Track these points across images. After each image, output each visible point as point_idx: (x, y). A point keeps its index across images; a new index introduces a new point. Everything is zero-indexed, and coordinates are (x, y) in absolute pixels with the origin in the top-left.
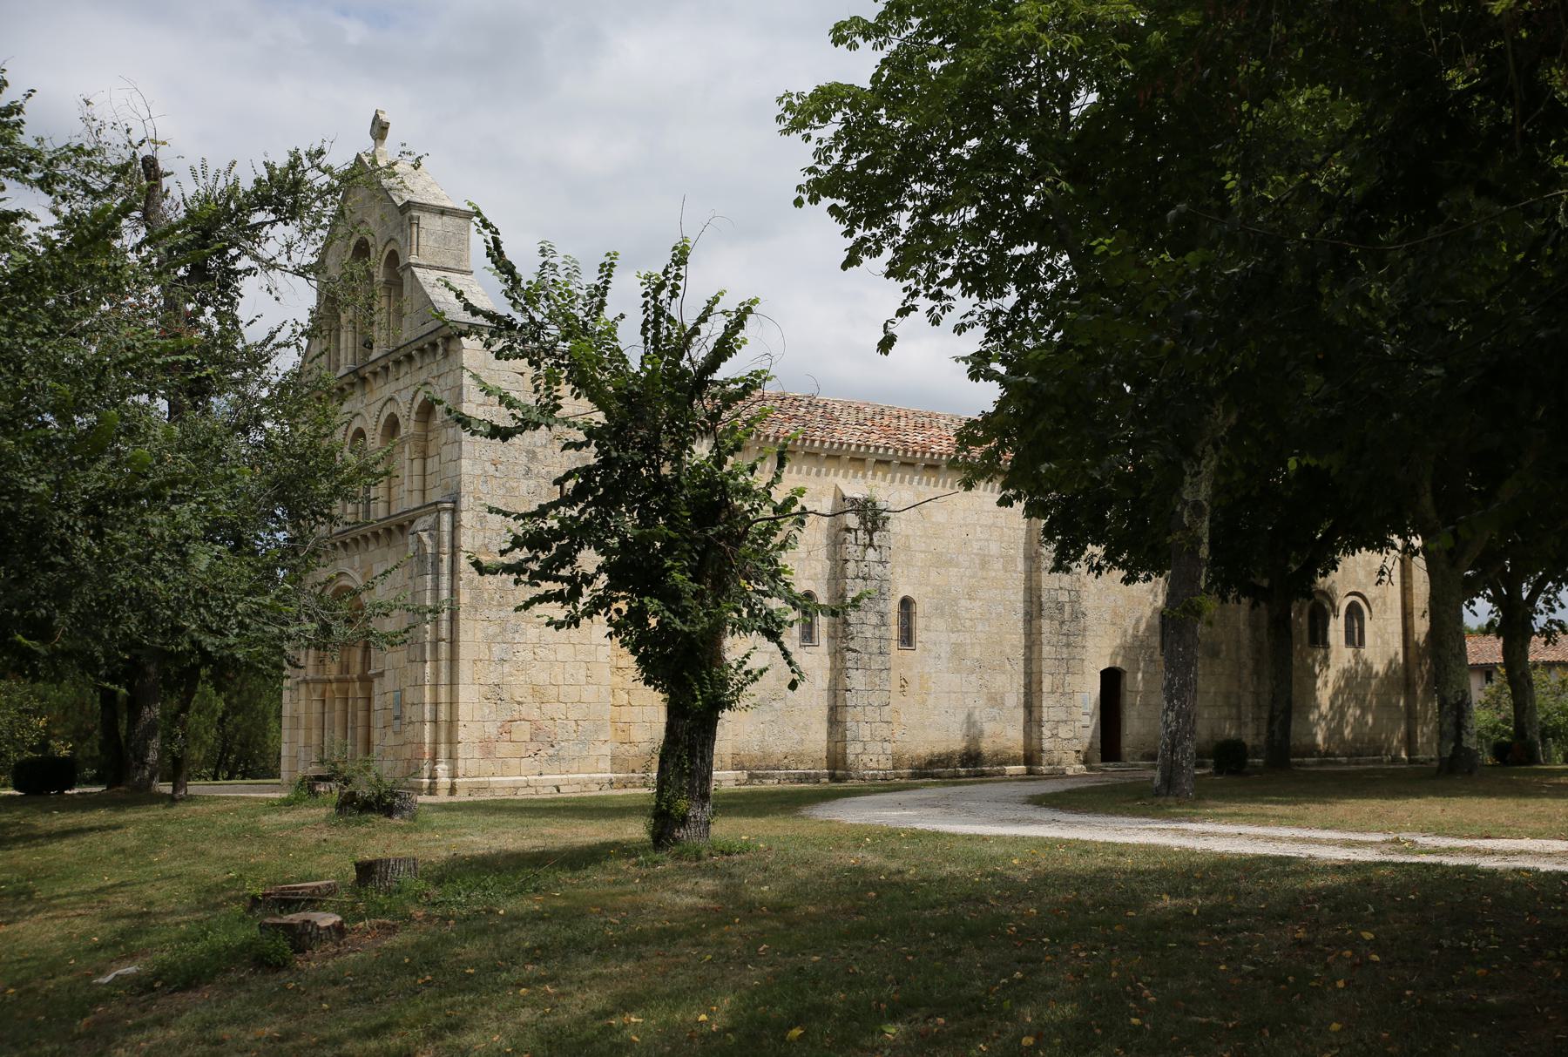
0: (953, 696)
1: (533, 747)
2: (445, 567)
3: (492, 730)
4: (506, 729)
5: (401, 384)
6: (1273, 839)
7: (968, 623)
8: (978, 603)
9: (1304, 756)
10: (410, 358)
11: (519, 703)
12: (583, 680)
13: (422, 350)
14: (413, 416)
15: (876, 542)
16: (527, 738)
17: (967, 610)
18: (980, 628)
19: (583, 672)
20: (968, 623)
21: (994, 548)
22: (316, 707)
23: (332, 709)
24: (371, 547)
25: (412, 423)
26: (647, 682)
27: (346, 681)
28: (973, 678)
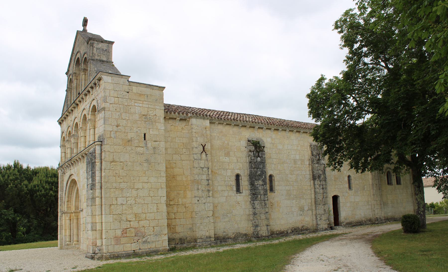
0: (288, 208)
1: (136, 238)
2: (98, 164)
3: (119, 233)
4: (125, 231)
5: (87, 102)
6: (67, 183)
7: (291, 183)
8: (294, 176)
9: (68, 197)
10: (89, 92)
11: (130, 221)
12: (156, 211)
13: (92, 88)
14: (90, 113)
15: (260, 155)
16: (134, 235)
17: (291, 178)
18: (295, 184)
19: (155, 207)
20: (291, 183)
21: (298, 157)
22: (68, 222)
23: (73, 222)
24: (79, 164)
25: (90, 115)
26: (16, 165)
27: (77, 212)
28: (294, 201)
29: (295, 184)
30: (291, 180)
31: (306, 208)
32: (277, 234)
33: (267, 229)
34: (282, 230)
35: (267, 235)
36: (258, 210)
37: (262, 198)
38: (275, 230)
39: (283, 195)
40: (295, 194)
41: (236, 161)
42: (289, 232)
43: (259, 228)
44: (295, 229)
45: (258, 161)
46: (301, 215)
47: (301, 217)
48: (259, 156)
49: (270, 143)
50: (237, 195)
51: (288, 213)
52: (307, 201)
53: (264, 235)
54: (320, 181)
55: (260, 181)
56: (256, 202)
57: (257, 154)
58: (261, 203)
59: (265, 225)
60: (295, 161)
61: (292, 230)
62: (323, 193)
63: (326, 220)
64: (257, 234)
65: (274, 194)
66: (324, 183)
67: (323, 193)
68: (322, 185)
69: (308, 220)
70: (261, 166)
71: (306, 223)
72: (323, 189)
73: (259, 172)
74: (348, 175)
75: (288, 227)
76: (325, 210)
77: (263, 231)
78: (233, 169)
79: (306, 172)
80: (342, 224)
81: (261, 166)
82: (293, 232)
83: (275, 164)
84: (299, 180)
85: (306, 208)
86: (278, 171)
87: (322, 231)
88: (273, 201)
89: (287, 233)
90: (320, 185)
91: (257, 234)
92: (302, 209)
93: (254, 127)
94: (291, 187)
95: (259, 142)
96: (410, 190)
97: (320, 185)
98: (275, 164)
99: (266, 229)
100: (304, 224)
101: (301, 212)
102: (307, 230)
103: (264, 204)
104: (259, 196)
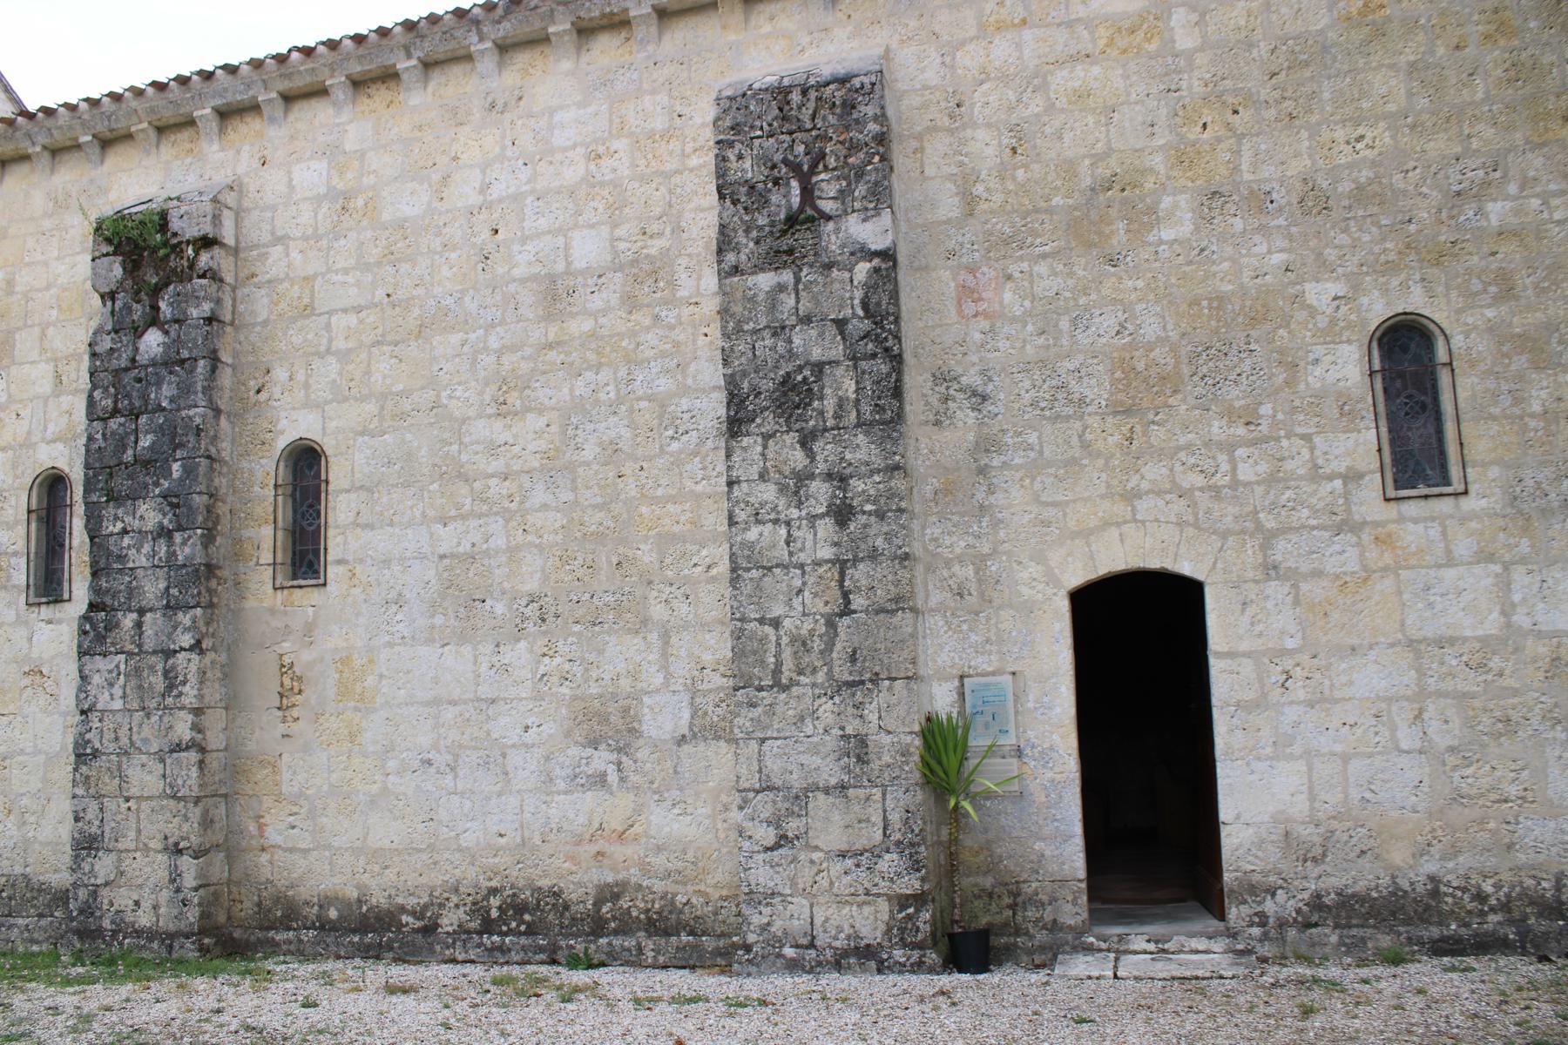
0: (449, 713)
7: (496, 488)
8: (534, 422)
17: (493, 449)
20: (496, 488)
28: (519, 654)
29: (539, 496)
30: (496, 465)
31: (664, 717)
32: (324, 926)
33: (175, 877)
34: (379, 899)
35: (167, 923)
36: (108, 724)
37: (149, 631)
38: (304, 892)
39: (399, 602)
40: (532, 585)
41: (46, 387)
42: (449, 921)
43: (103, 866)
44: (520, 909)
45: (142, 359)
46: (600, 780)
47: (590, 798)
48: (154, 320)
49: (319, 200)
50: (33, 614)
51: (441, 759)
52: (674, 658)
53: (144, 920)
54: (806, 442)
55: (144, 508)
56: (101, 666)
57: (138, 311)
58: (138, 671)
59: (155, 844)
60: (555, 294)
61: (479, 909)
62: (842, 565)
63: (875, 853)
64: (87, 910)
65: (315, 596)
66: (863, 449)
67: (842, 565)
68: (839, 479)
69: (677, 829)
70: (167, 391)
71: (659, 861)
72: (842, 514)
73: (146, 441)
74: (1378, 310)
75: (437, 878)
76: (858, 749)
77: (142, 888)
78: (27, 444)
79: (685, 359)
80: (1234, 913)
81: (167, 391)
82: (488, 926)
83: (344, 356)
84: (590, 452)
85: (664, 717)
86: (371, 407)
87: (794, 966)
88: (306, 656)
89: (430, 929)
90: (803, 477)
91: (87, 910)
92: (608, 727)
93: (190, 123)
94: (496, 525)
95: (164, 216)
96: (1372, 434)
97: (803, 477)
98: (344, 356)
99: (163, 874)
100: (634, 876)
101: (602, 759)
102: (662, 923)
103: (158, 682)
104: (128, 621)
